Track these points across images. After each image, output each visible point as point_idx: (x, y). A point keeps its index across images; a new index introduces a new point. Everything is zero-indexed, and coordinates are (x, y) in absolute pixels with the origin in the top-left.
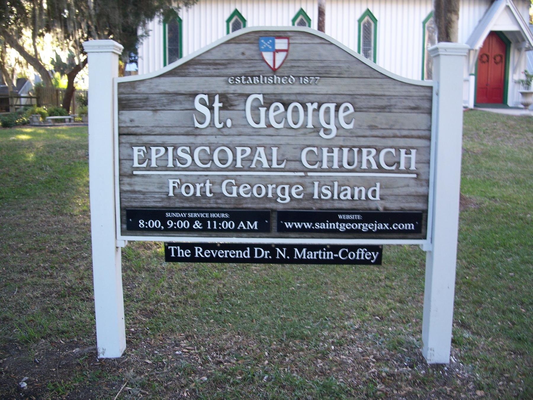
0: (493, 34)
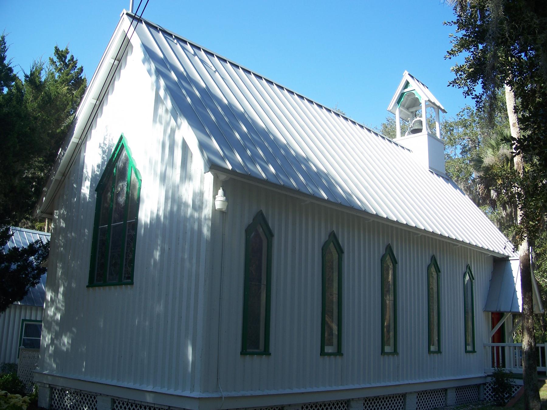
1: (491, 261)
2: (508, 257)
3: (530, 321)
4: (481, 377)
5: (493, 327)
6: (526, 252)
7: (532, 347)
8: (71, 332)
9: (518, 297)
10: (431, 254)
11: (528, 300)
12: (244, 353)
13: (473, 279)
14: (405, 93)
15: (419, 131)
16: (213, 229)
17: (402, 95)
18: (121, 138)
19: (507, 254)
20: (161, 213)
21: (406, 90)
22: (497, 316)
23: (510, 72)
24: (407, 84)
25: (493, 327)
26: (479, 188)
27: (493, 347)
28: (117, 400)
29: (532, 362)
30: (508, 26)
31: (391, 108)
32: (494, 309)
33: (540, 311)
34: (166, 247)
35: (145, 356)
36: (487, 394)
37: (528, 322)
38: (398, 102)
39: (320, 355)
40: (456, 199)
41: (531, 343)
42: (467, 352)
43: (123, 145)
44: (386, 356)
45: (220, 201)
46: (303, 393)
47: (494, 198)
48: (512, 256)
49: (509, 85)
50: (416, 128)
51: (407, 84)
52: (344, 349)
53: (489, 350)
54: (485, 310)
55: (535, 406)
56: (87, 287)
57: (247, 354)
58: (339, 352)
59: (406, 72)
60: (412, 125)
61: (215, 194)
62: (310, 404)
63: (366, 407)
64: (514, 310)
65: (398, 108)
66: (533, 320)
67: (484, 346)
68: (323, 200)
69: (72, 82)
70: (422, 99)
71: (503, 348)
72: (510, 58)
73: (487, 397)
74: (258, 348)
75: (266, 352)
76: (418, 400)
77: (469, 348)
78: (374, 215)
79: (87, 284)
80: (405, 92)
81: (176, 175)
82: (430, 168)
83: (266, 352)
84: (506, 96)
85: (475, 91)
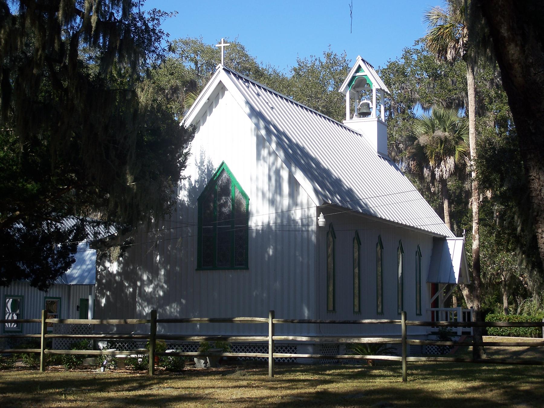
1: (434, 240)
2: (446, 237)
3: (478, 291)
4: (425, 335)
5: (432, 297)
8: (180, 303)
13: (421, 256)
14: (357, 77)
15: (365, 114)
16: (317, 238)
17: (353, 77)
18: (223, 163)
19: (445, 235)
20: (272, 222)
21: (358, 74)
22: (435, 288)
24: (359, 68)
25: (432, 297)
26: (412, 165)
27: (433, 312)
28: (239, 346)
31: (342, 91)
32: (435, 281)
33: (467, 281)
34: (279, 247)
36: (428, 349)
37: (477, 292)
38: (349, 85)
40: (388, 175)
41: (479, 306)
42: (417, 315)
43: (223, 169)
45: (322, 220)
47: (426, 176)
48: (450, 236)
50: (365, 111)
51: (359, 68)
53: (430, 313)
54: (428, 282)
56: (196, 270)
59: (359, 56)
60: (359, 106)
61: (318, 215)
64: (451, 282)
65: (349, 91)
67: (427, 311)
68: (360, 212)
70: (373, 85)
71: (437, 312)
73: (428, 351)
77: (418, 312)
78: (388, 220)
79: (196, 268)
80: (356, 75)
81: (286, 202)
82: (378, 152)
84: (470, 136)
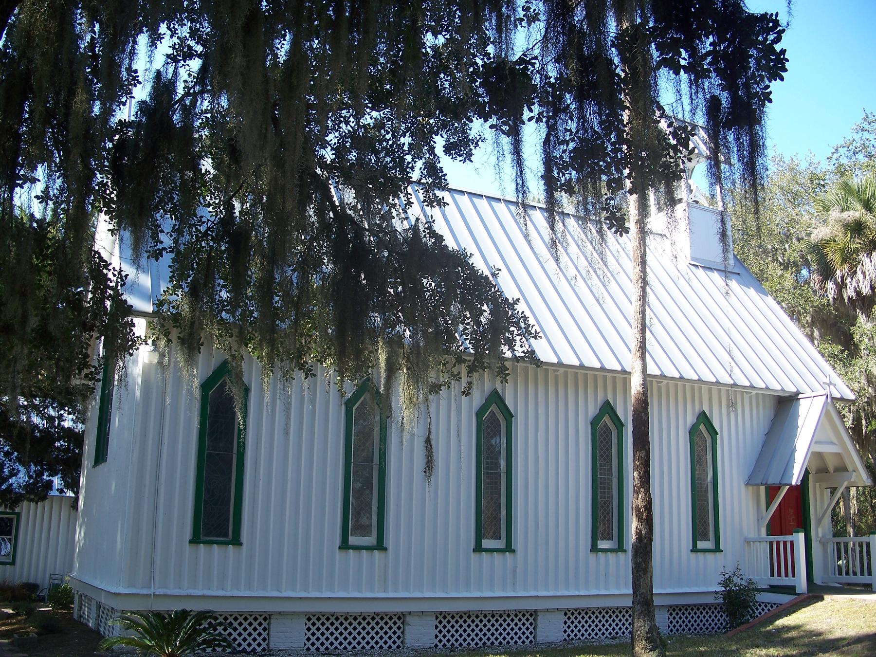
0: (813, 453)
3: (640, 496)
6: (638, 389)
7: (641, 537)
9: (796, 460)
10: (600, 400)
11: (638, 464)
12: (195, 540)
23: (616, 123)
29: (641, 560)
30: (31, 84)
35: (119, 545)
39: (591, 551)
41: (641, 531)
44: (700, 555)
46: (301, 598)
49: (334, 152)
52: (390, 540)
55: (641, 627)
57: (200, 543)
58: (380, 546)
62: (252, 614)
63: (671, 631)
66: (645, 495)
69: (63, 206)
72: (331, 114)
74: (226, 535)
75: (236, 541)
76: (671, 622)
83: (236, 541)
85: (460, 161)
